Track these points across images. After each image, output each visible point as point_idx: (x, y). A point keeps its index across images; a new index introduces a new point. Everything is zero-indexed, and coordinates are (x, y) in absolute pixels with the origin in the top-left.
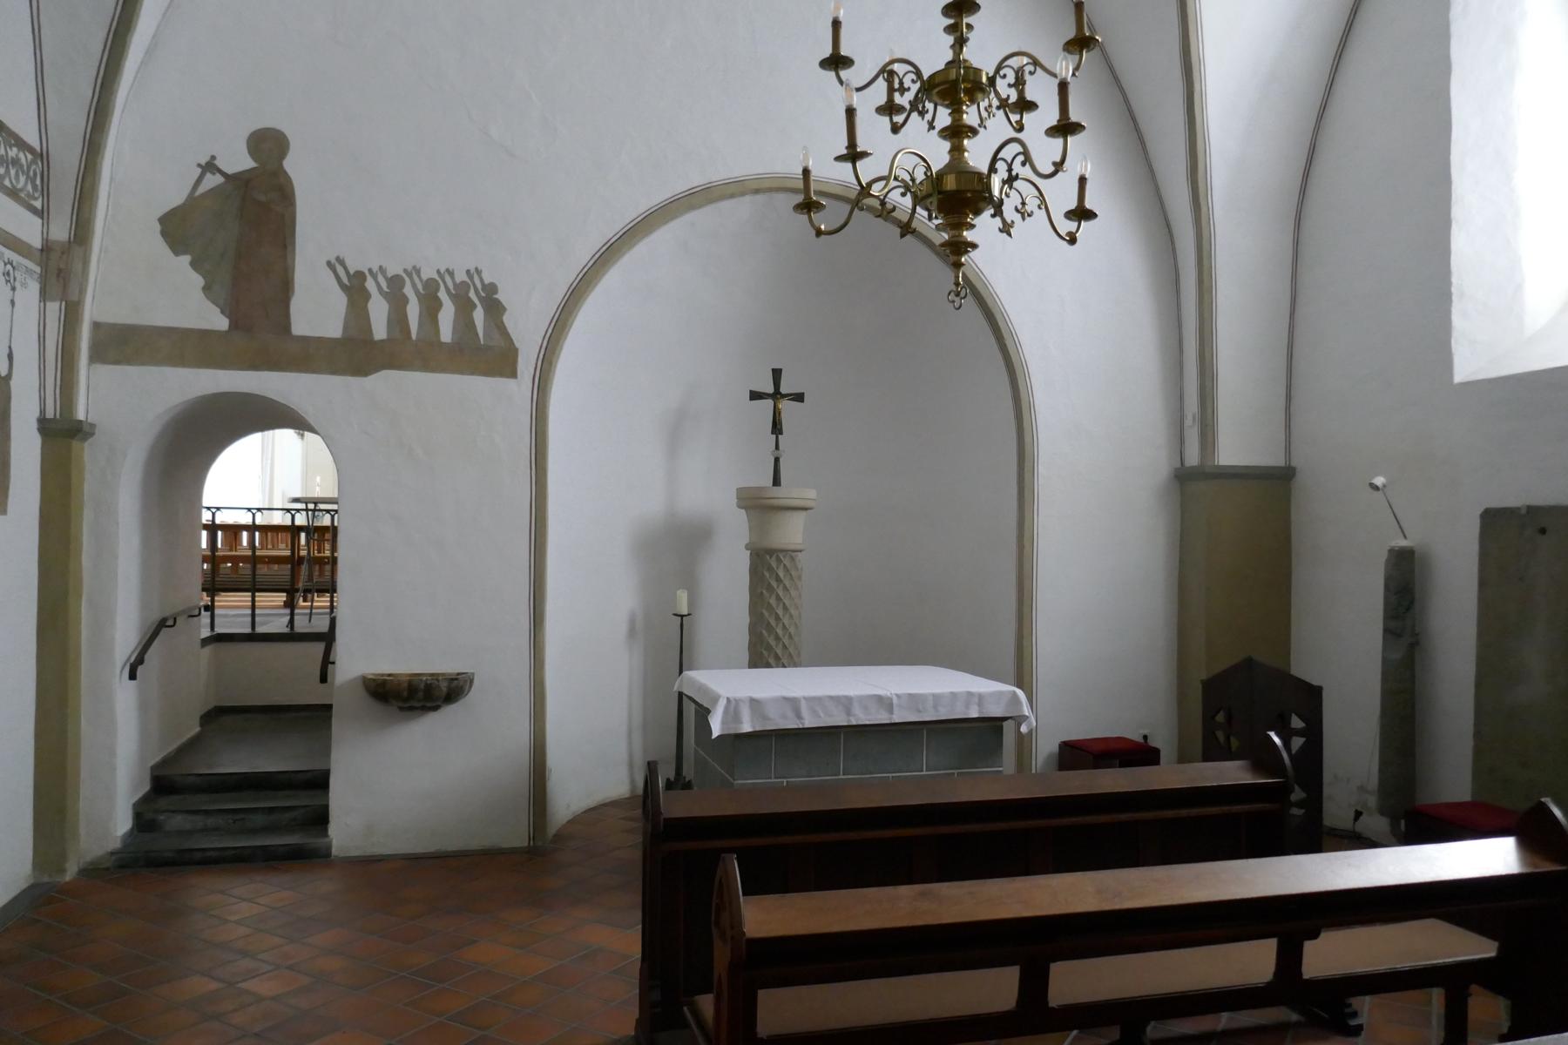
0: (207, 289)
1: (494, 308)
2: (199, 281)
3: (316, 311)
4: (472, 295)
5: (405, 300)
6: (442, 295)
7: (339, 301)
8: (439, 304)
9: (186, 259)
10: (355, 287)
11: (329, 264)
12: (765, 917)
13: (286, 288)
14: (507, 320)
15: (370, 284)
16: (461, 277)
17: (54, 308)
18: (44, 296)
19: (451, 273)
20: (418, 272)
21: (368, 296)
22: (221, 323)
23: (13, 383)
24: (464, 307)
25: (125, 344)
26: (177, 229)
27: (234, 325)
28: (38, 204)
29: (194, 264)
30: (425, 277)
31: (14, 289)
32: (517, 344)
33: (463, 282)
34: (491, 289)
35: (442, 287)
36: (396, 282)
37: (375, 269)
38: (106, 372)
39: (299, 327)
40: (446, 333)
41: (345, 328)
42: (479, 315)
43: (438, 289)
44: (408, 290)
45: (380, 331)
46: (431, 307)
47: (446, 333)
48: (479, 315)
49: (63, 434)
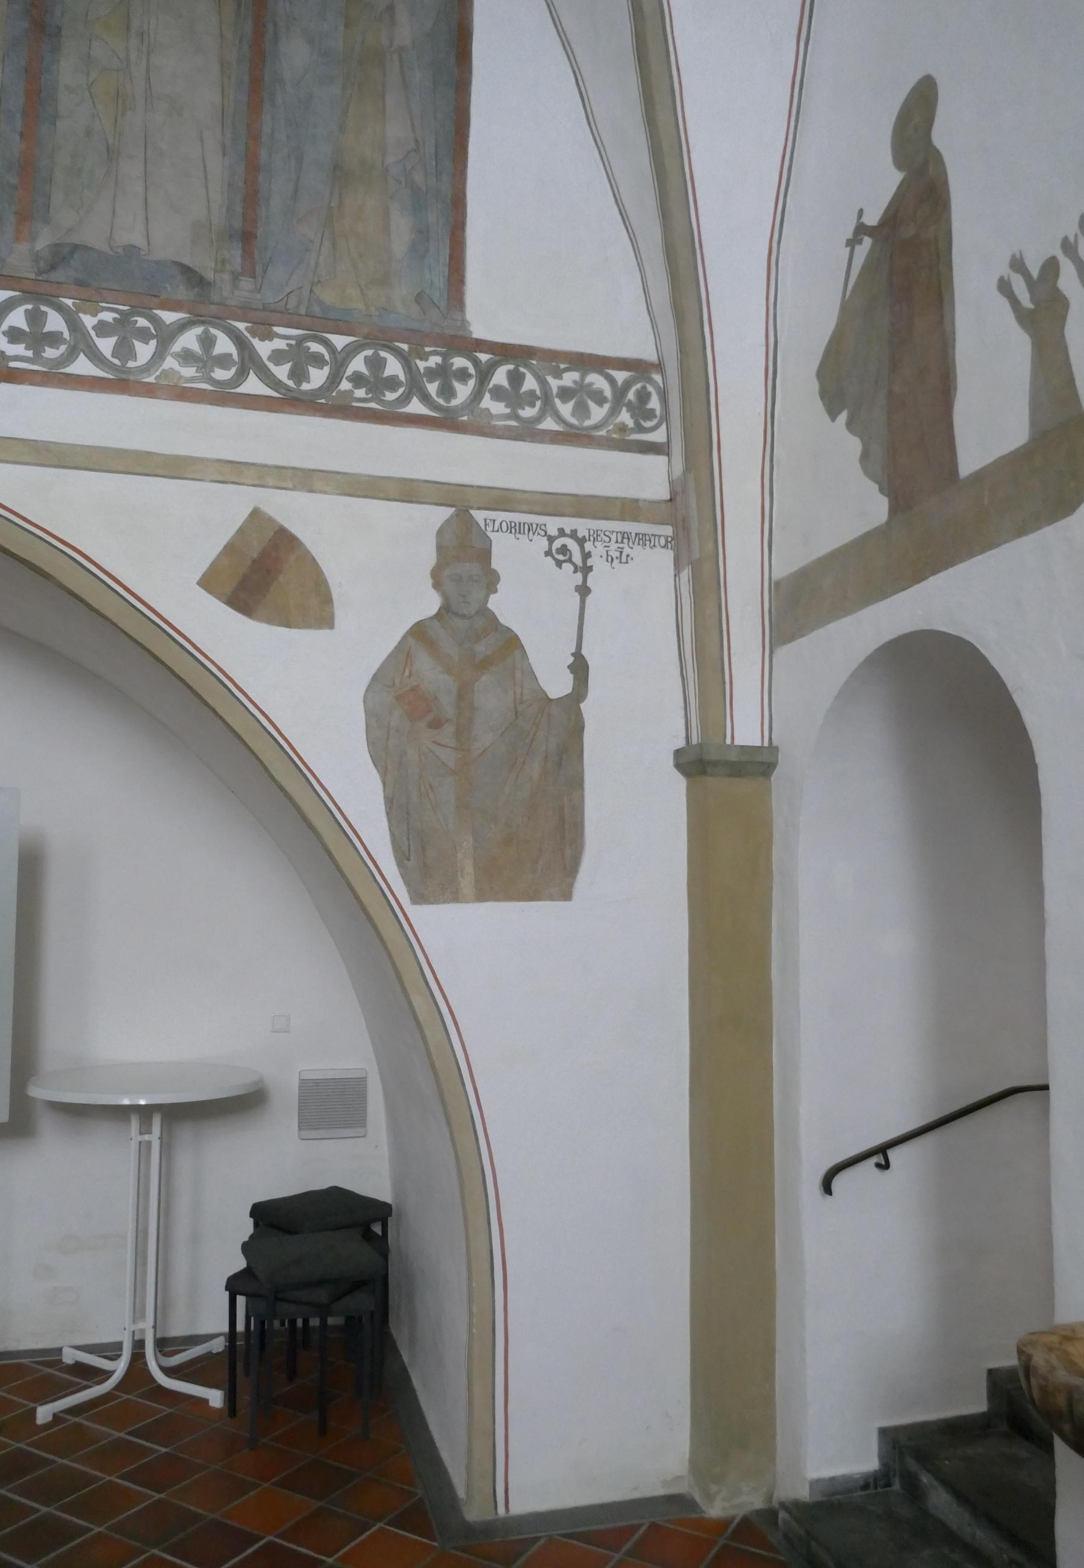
17: (685, 575)
28: (658, 436)
29: (850, 425)
49: (722, 776)
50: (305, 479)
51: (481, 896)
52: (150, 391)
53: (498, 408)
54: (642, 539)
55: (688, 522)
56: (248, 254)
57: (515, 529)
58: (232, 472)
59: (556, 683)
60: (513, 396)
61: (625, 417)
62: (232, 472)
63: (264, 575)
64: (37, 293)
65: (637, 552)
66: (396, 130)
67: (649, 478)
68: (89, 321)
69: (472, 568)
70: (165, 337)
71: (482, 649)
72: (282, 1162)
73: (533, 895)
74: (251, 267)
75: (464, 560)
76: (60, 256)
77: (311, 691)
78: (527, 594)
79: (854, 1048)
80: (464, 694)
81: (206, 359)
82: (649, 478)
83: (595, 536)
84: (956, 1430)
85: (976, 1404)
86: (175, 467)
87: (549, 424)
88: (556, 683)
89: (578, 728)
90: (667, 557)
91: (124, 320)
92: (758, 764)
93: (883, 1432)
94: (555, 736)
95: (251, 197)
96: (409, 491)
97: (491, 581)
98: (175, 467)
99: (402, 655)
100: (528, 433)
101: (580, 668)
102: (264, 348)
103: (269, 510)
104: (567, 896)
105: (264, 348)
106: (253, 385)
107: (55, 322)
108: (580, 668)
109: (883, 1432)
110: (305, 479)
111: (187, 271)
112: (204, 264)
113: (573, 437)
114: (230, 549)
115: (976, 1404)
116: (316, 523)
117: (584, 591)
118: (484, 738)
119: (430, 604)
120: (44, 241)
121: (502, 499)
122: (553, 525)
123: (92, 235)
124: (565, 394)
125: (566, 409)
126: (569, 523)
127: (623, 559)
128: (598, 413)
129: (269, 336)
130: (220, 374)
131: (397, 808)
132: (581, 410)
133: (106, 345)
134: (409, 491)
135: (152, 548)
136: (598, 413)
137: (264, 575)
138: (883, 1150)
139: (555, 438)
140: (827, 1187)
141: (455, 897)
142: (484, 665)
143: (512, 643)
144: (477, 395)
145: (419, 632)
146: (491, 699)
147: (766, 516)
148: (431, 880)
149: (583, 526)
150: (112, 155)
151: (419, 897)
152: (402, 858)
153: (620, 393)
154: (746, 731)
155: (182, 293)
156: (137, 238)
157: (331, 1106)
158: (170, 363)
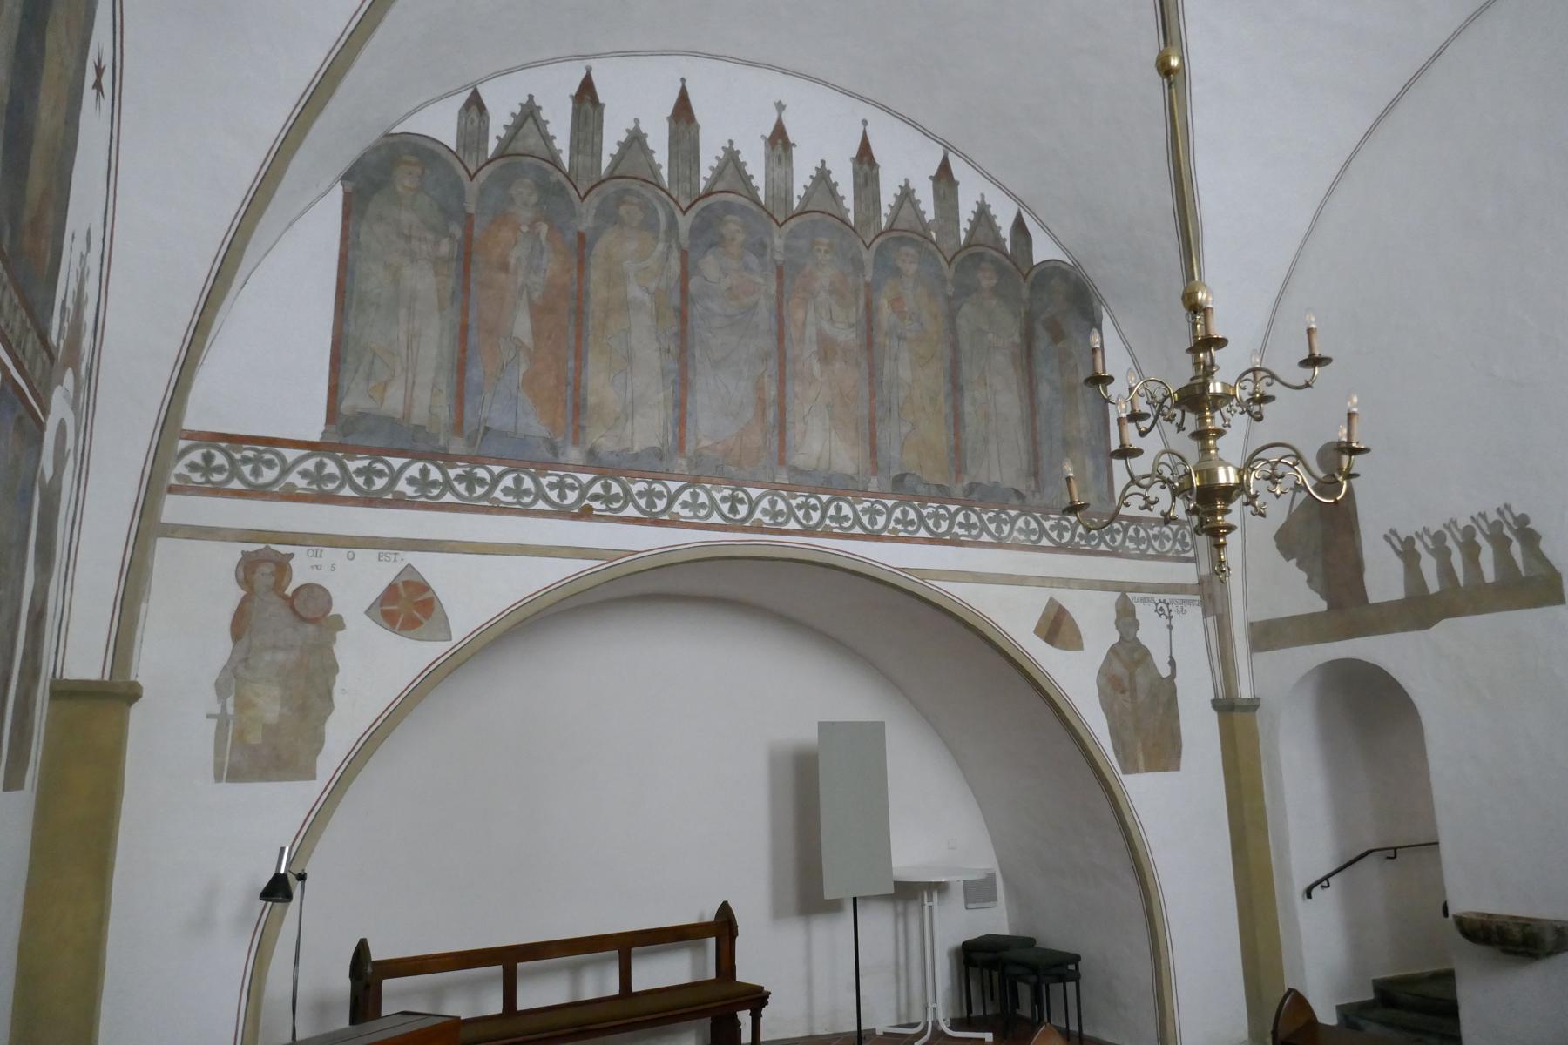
0: (1309, 581)
1: (1529, 538)
2: (1303, 576)
3: (1383, 580)
4: (1506, 531)
5: (1448, 552)
6: (1480, 539)
7: (1398, 565)
8: (1477, 548)
9: (1294, 561)
10: (1408, 553)
11: (1387, 538)
12: (996, 974)
13: (1358, 567)
14: (1544, 546)
15: (1419, 546)
16: (1493, 517)
17: (1211, 620)
18: (1205, 616)
19: (1483, 516)
20: (1455, 523)
21: (1418, 556)
22: (1321, 605)
23: (1176, 681)
24: (1501, 544)
25: (1267, 636)
26: (314, 777)
27: (1330, 607)
28: (1191, 554)
29: (1298, 565)
30: (1461, 525)
31: (1170, 617)
32: (1558, 568)
33: (1496, 522)
34: (1523, 520)
35: (1448, 535)
36: (1439, 538)
37: (1420, 531)
38: (1262, 658)
39: (1375, 595)
40: (1489, 574)
41: (1407, 589)
42: (1516, 549)
43: (1474, 536)
44: (1450, 543)
45: (1433, 586)
46: (1471, 551)
47: (1489, 574)
48: (1516, 549)
49: (1232, 710)
50: (1067, 583)
51: (1150, 768)
52: (1009, 547)
53: (1131, 545)
54: (1190, 602)
55: (1211, 594)
56: (1037, 482)
57: (1144, 600)
58: (1043, 581)
59: (1165, 671)
60: (1137, 540)
61: (1178, 547)
62: (1043, 581)
63: (1057, 627)
64: (967, 506)
65: (1188, 608)
66: (1083, 421)
67: (1187, 574)
68: (985, 517)
69: (1129, 619)
70: (1013, 521)
71: (1136, 656)
72: (957, 924)
73: (1166, 769)
74: (1039, 488)
75: (1126, 617)
76: (972, 487)
77: (1076, 677)
78: (1151, 632)
79: (1306, 836)
80: (1132, 677)
81: (1027, 532)
82: (1187, 574)
83: (1172, 601)
84: (1363, 1007)
85: (1369, 995)
86: (1021, 581)
87: (1151, 552)
88: (1165, 671)
89: (1174, 691)
90: (1198, 611)
91: (998, 514)
92: (1252, 705)
93: (1339, 1007)
94: (1165, 694)
95: (1035, 456)
96: (1104, 586)
97: (1136, 625)
98: (1021, 581)
99: (1108, 660)
100: (1143, 556)
101: (1172, 663)
102: (1047, 524)
103: (1056, 598)
104: (1178, 769)
105: (1047, 524)
106: (1045, 542)
107: (974, 518)
108: (1172, 663)
109: (1339, 1007)
110: (1067, 583)
111: (1016, 491)
112: (1022, 487)
113: (1160, 557)
114: (1043, 616)
115: (1369, 995)
116: (1072, 601)
117: (1170, 627)
118: (1141, 697)
119: (1116, 637)
120: (966, 483)
121: (1138, 587)
122: (1157, 597)
123: (983, 479)
124: (1156, 537)
125: (1156, 544)
126: (1162, 597)
127: (1183, 612)
128: (1168, 545)
129: (1048, 519)
130: (1034, 538)
131: (1114, 732)
132: (1162, 545)
133: (992, 527)
134: (1104, 586)
135: (1014, 616)
136: (1168, 545)
137: (1057, 627)
138: (1326, 878)
139: (1153, 558)
140: (1309, 896)
141: (1137, 771)
142: (1138, 663)
143: (1147, 653)
144: (1124, 541)
145: (1113, 650)
146: (1142, 680)
147: (1245, 593)
148: (1130, 767)
149: (1167, 597)
150: (986, 441)
151: (1125, 772)
152: (1117, 753)
153: (1175, 535)
154: (1245, 692)
155: (1015, 501)
156: (995, 477)
157: (978, 892)
158: (1015, 534)
